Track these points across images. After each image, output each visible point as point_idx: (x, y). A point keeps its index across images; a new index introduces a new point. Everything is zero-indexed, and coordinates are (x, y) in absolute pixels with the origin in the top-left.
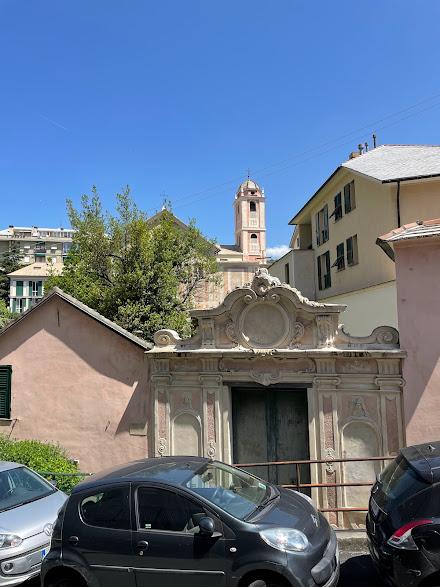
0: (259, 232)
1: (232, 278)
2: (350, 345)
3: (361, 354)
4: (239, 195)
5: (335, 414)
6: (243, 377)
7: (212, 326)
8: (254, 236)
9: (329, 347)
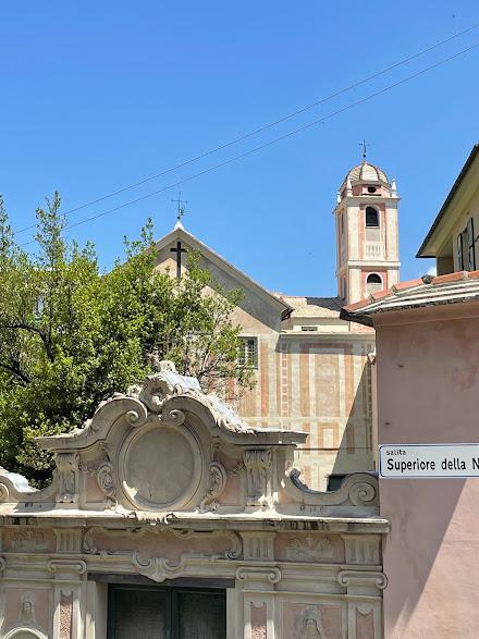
0: (384, 269)
1: (318, 365)
2: (303, 507)
3: (314, 524)
4: (343, 195)
5: (271, 626)
6: (122, 564)
7: (75, 467)
8: (374, 279)
9: (269, 507)
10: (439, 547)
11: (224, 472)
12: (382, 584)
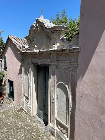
10: (93, 55)
11: (48, 40)
12: (78, 67)
